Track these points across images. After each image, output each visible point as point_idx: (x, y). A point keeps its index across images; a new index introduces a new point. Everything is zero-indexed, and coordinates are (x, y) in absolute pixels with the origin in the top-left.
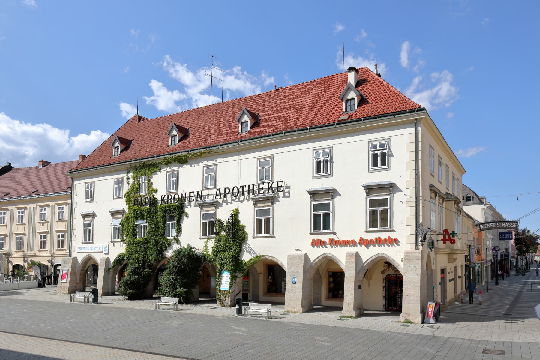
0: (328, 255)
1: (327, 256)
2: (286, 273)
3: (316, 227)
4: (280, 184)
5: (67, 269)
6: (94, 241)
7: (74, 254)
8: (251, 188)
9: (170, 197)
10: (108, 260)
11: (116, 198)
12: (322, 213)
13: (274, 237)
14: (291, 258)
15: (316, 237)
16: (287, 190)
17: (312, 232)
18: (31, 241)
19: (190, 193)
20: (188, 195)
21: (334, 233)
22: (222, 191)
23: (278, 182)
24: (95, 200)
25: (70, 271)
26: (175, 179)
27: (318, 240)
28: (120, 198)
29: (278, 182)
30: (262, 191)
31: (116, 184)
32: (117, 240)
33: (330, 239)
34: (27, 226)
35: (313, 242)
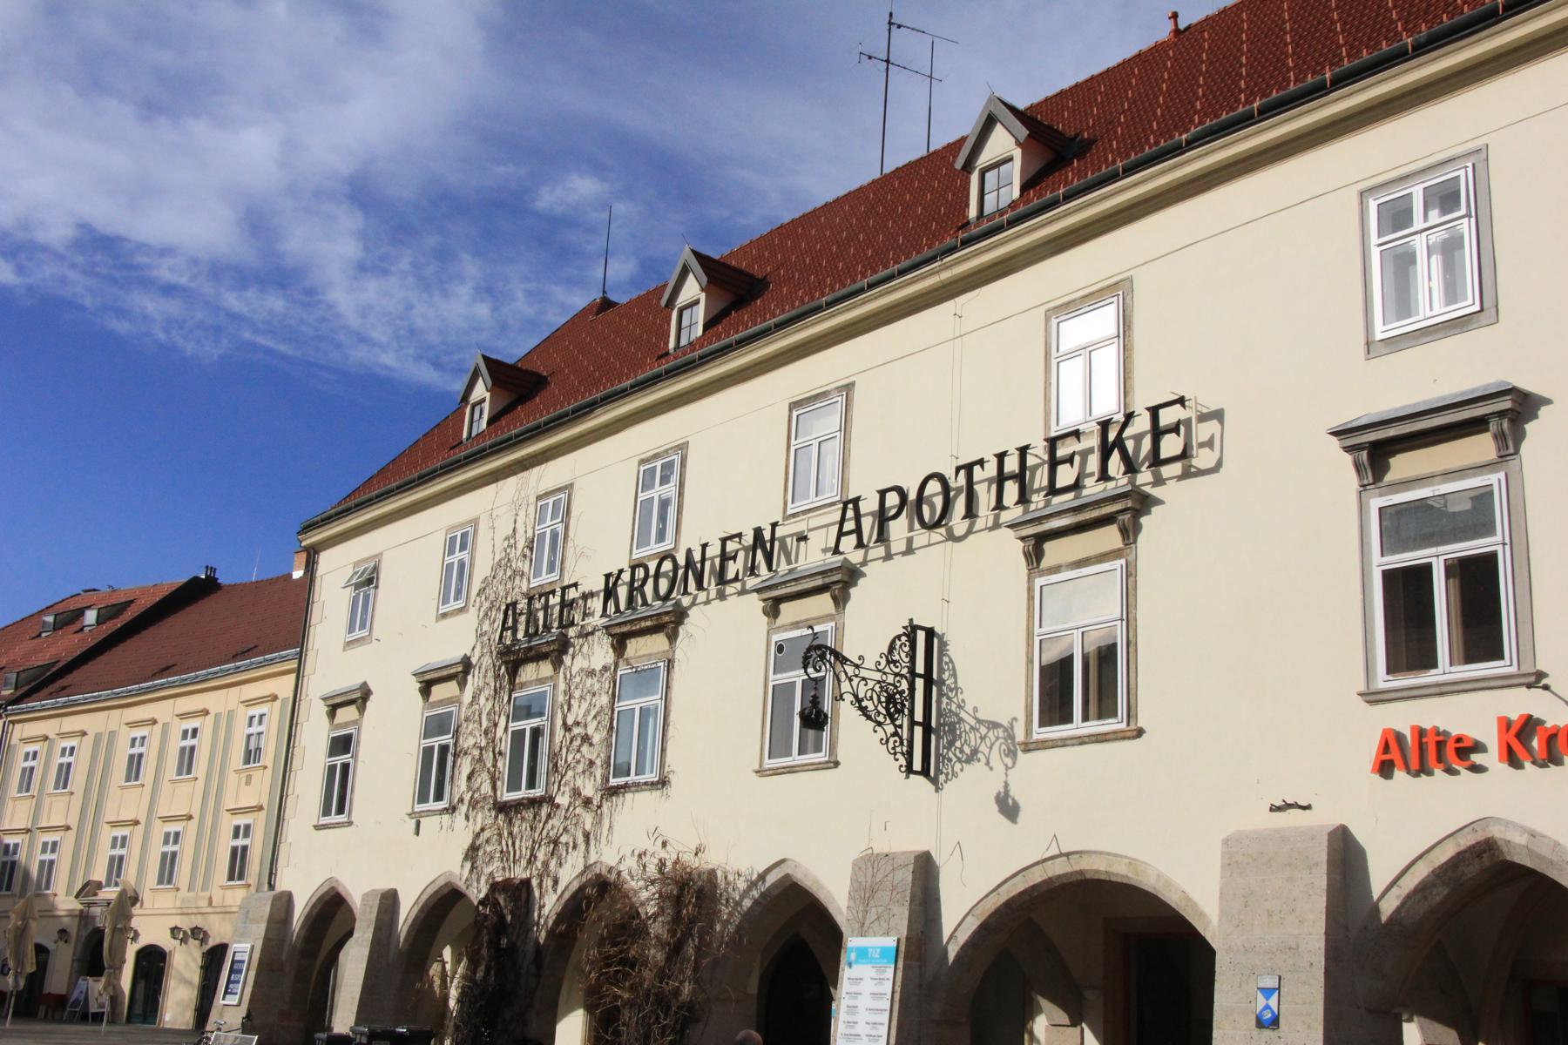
0: (1496, 832)
1: (1487, 847)
2: (1211, 953)
3: (1409, 639)
4: (1167, 417)
5: (248, 946)
6: (353, 818)
7: (282, 884)
8: (1012, 465)
9: (640, 573)
10: (389, 900)
11: (444, 615)
12: (1437, 557)
13: (1140, 733)
14: (1242, 857)
15: (1404, 718)
16: (1202, 432)
17: (1383, 680)
18: (206, 843)
19: (724, 541)
20: (714, 551)
21: (1537, 680)
22: (869, 505)
23: (1154, 411)
24: (375, 635)
25: (256, 956)
26: (670, 490)
27: (1420, 733)
28: (461, 610)
29: (1154, 411)
30: (1066, 475)
31: (451, 552)
32: (432, 805)
33: (1505, 724)
34: (200, 784)
35: (1385, 748)
